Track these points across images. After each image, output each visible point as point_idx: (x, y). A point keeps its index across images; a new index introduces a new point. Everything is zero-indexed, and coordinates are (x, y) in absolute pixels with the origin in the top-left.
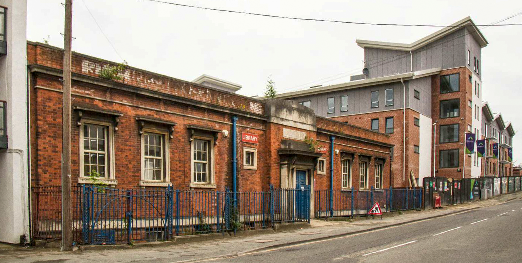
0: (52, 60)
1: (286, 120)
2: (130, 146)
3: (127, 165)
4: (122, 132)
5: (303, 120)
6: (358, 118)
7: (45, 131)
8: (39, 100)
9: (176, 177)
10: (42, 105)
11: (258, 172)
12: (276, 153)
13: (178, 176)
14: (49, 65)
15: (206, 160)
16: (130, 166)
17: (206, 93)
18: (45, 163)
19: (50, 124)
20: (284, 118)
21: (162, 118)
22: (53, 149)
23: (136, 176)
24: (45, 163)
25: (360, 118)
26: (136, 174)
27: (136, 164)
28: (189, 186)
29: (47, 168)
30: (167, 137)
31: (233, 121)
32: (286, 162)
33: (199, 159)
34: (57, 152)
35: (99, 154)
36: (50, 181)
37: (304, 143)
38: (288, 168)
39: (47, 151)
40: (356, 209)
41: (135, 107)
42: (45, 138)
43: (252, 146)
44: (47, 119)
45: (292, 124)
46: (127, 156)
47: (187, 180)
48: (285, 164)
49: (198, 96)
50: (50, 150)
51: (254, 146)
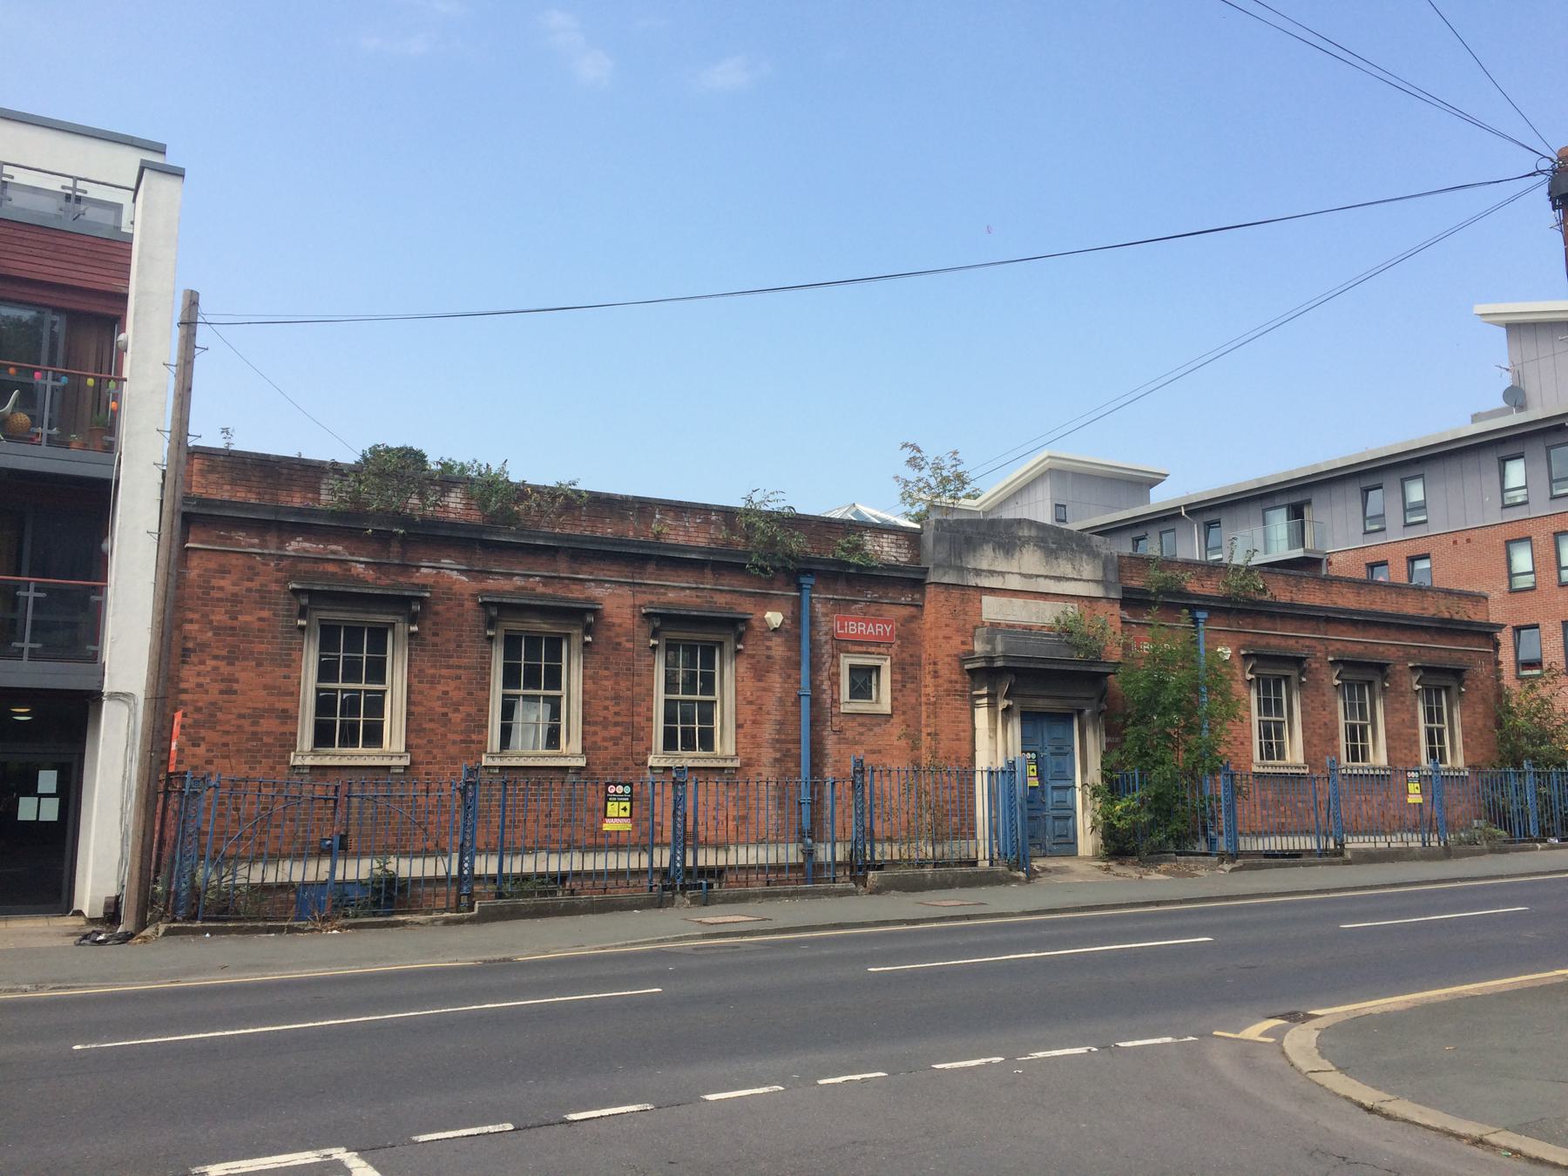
0: (233, 483)
1: (992, 573)
2: (459, 667)
3: (445, 714)
4: (435, 634)
5: (1065, 568)
6: (1461, 540)
7: (203, 646)
8: (193, 574)
9: (604, 739)
10: (199, 587)
11: (895, 720)
12: (955, 665)
13: (612, 739)
14: (226, 496)
15: (713, 694)
16: (456, 717)
17: (707, 522)
18: (196, 721)
19: (218, 630)
20: (985, 566)
21: (561, 593)
22: (223, 686)
23: (473, 742)
24: (196, 721)
25: (1468, 541)
26: (474, 737)
27: (473, 710)
28: (645, 763)
29: (203, 733)
30: (1294, 682)
31: (799, 588)
32: (984, 691)
33: (690, 687)
34: (235, 692)
35: (367, 691)
36: (209, 762)
37: (1065, 631)
38: (992, 706)
39: (207, 692)
40: (517, 852)
41: (481, 572)
42: (202, 663)
43: (872, 649)
44: (212, 617)
45: (1014, 583)
46: (446, 693)
47: (639, 748)
48: (981, 697)
49: (678, 535)
50: (214, 689)
51: (882, 650)
